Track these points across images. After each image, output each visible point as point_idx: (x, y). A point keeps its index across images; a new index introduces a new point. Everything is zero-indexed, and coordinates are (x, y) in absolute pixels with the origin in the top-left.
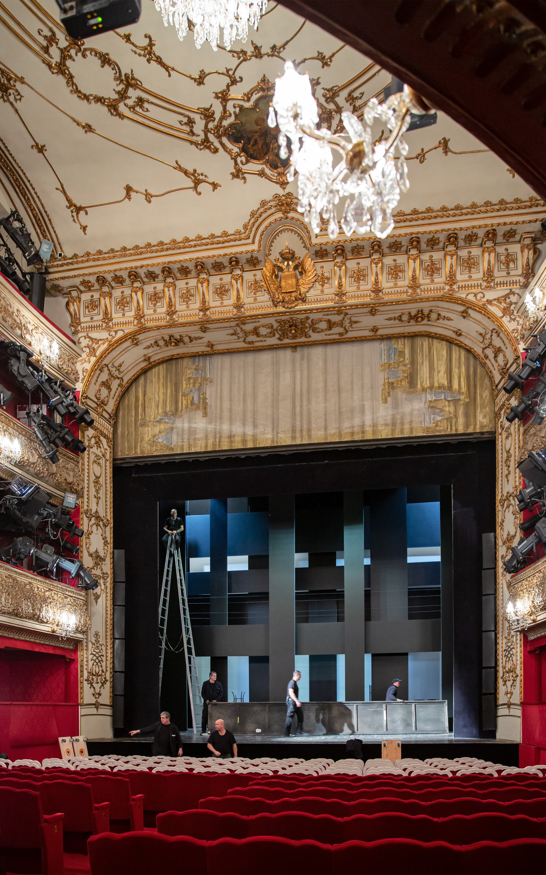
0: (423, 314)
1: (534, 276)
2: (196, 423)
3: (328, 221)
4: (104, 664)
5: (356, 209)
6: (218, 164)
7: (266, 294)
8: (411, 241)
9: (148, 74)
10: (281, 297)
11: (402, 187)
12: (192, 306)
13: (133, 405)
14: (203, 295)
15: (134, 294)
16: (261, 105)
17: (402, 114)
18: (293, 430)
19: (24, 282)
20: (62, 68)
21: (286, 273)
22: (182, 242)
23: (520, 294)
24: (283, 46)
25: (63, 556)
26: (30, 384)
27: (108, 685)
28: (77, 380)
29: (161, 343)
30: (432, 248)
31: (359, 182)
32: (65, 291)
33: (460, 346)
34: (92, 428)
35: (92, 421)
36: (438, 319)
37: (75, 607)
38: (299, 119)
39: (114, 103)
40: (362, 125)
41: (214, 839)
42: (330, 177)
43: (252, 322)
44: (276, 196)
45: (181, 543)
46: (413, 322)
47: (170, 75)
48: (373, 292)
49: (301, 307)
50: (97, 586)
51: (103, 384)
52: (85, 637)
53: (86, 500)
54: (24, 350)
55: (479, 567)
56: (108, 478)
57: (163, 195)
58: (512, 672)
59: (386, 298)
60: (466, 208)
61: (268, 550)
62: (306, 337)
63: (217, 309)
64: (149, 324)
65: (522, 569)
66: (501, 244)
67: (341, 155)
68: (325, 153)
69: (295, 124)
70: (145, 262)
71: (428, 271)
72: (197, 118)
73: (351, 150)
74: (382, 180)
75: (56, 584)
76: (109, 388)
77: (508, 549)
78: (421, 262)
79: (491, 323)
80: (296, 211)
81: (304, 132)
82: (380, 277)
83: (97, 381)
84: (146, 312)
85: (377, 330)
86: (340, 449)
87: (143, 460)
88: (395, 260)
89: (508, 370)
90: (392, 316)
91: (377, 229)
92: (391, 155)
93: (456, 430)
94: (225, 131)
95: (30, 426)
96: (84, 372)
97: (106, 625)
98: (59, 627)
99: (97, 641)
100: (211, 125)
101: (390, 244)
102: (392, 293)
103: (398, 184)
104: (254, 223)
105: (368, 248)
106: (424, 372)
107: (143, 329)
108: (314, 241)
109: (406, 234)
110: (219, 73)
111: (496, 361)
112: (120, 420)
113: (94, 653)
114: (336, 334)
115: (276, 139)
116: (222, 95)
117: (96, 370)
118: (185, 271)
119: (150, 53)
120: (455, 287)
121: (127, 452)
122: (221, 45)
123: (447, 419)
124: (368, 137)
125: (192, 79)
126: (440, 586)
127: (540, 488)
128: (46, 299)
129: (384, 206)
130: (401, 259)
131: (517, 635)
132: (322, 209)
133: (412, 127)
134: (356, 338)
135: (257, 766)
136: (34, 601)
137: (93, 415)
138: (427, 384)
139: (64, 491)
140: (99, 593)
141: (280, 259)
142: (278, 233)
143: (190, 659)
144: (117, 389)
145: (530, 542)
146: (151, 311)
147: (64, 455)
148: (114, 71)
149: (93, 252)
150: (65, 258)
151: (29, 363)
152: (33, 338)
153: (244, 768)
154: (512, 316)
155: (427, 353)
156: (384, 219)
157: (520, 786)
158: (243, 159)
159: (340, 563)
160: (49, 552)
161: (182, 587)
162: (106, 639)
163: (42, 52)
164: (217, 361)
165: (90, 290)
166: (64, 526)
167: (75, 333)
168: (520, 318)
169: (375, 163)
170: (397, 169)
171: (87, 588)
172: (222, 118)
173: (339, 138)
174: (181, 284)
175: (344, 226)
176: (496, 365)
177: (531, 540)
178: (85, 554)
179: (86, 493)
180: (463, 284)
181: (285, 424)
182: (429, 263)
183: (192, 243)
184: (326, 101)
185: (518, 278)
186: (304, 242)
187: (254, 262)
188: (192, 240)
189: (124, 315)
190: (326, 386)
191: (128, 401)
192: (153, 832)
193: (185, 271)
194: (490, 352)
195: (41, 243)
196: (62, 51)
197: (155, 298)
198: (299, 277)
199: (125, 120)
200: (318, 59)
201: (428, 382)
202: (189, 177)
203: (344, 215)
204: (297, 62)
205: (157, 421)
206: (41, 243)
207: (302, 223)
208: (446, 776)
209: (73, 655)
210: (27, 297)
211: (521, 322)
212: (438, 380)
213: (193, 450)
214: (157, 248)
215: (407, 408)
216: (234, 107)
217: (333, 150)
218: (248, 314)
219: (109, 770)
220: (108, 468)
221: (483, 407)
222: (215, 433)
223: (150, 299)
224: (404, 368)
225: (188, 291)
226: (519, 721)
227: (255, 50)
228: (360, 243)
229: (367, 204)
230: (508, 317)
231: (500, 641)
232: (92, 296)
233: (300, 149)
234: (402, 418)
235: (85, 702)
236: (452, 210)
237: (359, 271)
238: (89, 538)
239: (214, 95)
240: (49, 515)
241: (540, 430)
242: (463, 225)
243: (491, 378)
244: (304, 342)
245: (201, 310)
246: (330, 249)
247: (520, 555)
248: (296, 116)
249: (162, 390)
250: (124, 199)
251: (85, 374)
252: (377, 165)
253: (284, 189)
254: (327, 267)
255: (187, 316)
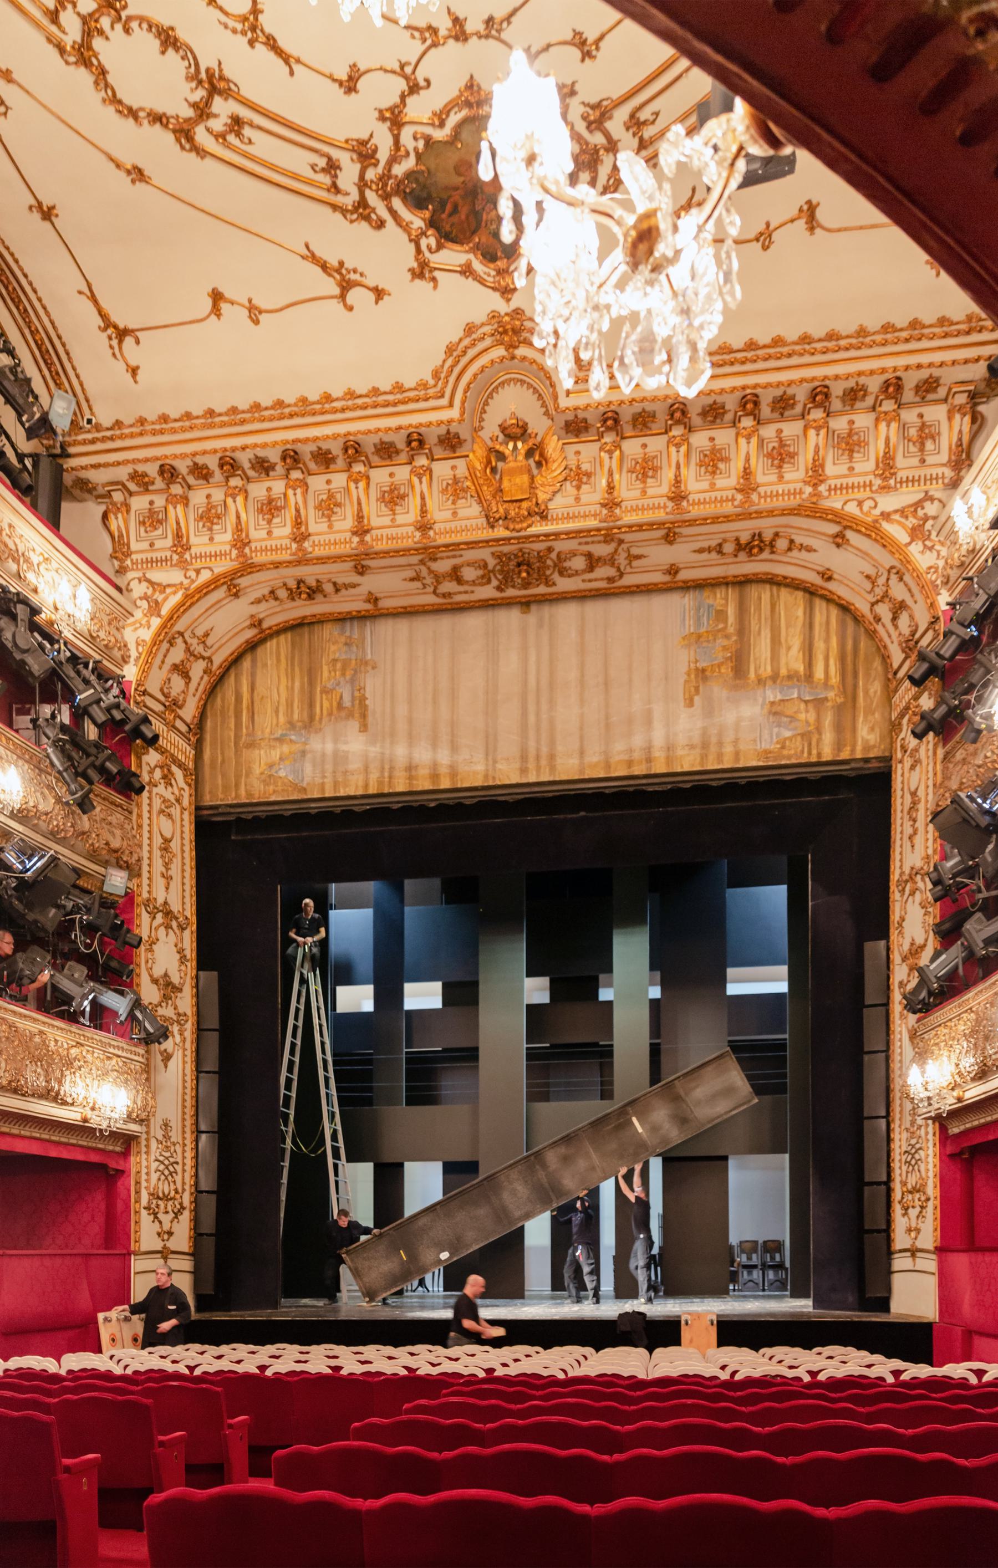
0: (762, 541)
1: (970, 466)
2: (346, 743)
3: (590, 363)
4: (178, 1179)
5: (641, 340)
6: (384, 250)
7: (474, 504)
8: (743, 403)
9: (250, 69)
10: (501, 510)
11: (728, 299)
12: (338, 526)
13: (232, 707)
14: (359, 504)
15: (230, 500)
16: (465, 135)
17: (730, 156)
18: (522, 757)
19: (21, 471)
20: (86, 54)
21: (512, 464)
22: (318, 402)
23: (944, 499)
24: (508, 19)
25: (102, 983)
26: (36, 666)
27: (186, 1216)
28: (125, 659)
29: (283, 594)
30: (782, 414)
31: (649, 289)
32: (100, 490)
33: (830, 599)
34: (156, 750)
35: (156, 737)
36: (790, 549)
37: (125, 1075)
38: (536, 164)
39: (186, 127)
40: (655, 177)
41: (378, 1497)
42: (593, 279)
43: (448, 557)
44: (494, 316)
45: (321, 959)
46: (742, 556)
47: (292, 73)
48: (671, 499)
49: (539, 528)
50: (167, 1037)
51: (175, 668)
52: (144, 1129)
53: (145, 881)
54: (25, 602)
55: (858, 1004)
56: (187, 842)
57: (281, 309)
58: (918, 1191)
59: (695, 512)
60: (848, 337)
61: (477, 973)
62: (547, 584)
63: (385, 532)
64: (259, 559)
65: (936, 1005)
66: (911, 405)
67: (614, 236)
68: (585, 231)
69: (530, 175)
70: (250, 440)
71: (773, 459)
72: (344, 158)
73: (635, 227)
74: (691, 284)
75: (91, 1032)
76: (186, 676)
77: (911, 969)
78: (761, 442)
79: (888, 555)
80: (530, 344)
81: (547, 191)
82: (683, 471)
83: (163, 662)
84: (254, 534)
85: (676, 572)
86: (607, 791)
87: (250, 809)
88: (712, 439)
89: (917, 643)
90: (705, 544)
91: (680, 381)
92: (708, 235)
93: (819, 755)
94: (398, 185)
95: (38, 743)
96: (138, 644)
97: (184, 1107)
98: (96, 1113)
99: (167, 1137)
100: (371, 174)
101: (703, 408)
102: (705, 502)
103: (721, 294)
104: (452, 367)
105: (662, 416)
106: (761, 649)
107: (248, 568)
108: (564, 402)
109: (735, 388)
110: (386, 71)
111: (896, 627)
112: (208, 737)
113: (161, 1158)
114: (602, 579)
115: (493, 202)
116: (393, 113)
117: (161, 641)
118: (324, 459)
119: (253, 28)
120: (822, 488)
121: (220, 794)
122: (390, 15)
123: (802, 735)
124: (666, 200)
125: (334, 80)
126: (787, 1036)
127: (973, 858)
128: (66, 506)
129: (694, 336)
130: (724, 436)
131: (927, 1125)
132: (580, 341)
133: (750, 180)
134: (638, 586)
135: (457, 1360)
136: (49, 1065)
137: (158, 726)
138: (767, 670)
139: (105, 864)
140: (170, 1050)
141: (501, 437)
142: (497, 388)
143: (336, 1166)
144: (202, 678)
145: (954, 956)
146: (263, 534)
147: (104, 799)
148: (186, 63)
149: (152, 417)
150: (98, 428)
151: (34, 627)
152: (41, 579)
153: (433, 1365)
154: (928, 543)
155: (769, 613)
156: (693, 359)
157: (935, 1399)
158: (432, 241)
159: (605, 994)
160: (76, 975)
161: (323, 1040)
162: (184, 1132)
163: (45, 22)
164: (386, 628)
165: (147, 490)
166: (106, 929)
167: (121, 571)
168: (942, 544)
169: (678, 252)
170: (719, 263)
171: (148, 1040)
172: (393, 160)
173: (610, 203)
174: (317, 483)
175: (618, 375)
176: (894, 634)
177: (955, 954)
178: (145, 980)
179: (145, 868)
180: (838, 482)
181: (508, 747)
182: (776, 445)
183: (337, 404)
184: (588, 128)
185: (940, 471)
186: (544, 405)
187: (451, 442)
188: (337, 399)
189: (211, 539)
190: (583, 675)
191: (223, 701)
192: (266, 1485)
193: (324, 459)
194: (884, 610)
195: (52, 397)
196: (85, 20)
197: (270, 508)
198: (535, 471)
199: (208, 161)
200: (574, 45)
201: (769, 668)
202: (330, 275)
203: (619, 353)
204: (533, 50)
205: (276, 739)
206: (52, 397)
207: (542, 368)
208: (798, 1379)
209: (121, 1162)
210: (28, 500)
211: (944, 552)
212: (787, 664)
213: (342, 793)
214: (272, 412)
215: (729, 716)
216: (415, 138)
217: (601, 229)
218: (441, 540)
219: (187, 1372)
220: (186, 823)
221: (869, 711)
222: (382, 761)
223: (260, 511)
224: (725, 642)
225: (331, 496)
226: (932, 1283)
227: (454, 26)
228: (649, 407)
229: (661, 332)
230: (920, 543)
231: (896, 1135)
232: (151, 503)
233: (538, 225)
234: (720, 735)
235: (143, 1249)
236: (820, 340)
237: (645, 460)
238: (151, 950)
239: (376, 114)
240: (76, 909)
241: (975, 754)
242: (839, 370)
243: (886, 659)
244: (543, 595)
245: (355, 533)
246: (592, 417)
247: (934, 980)
248: (531, 160)
249: (284, 680)
250: (208, 316)
251: (140, 649)
252: (683, 255)
253: (508, 300)
254: (587, 452)
255: (330, 543)
